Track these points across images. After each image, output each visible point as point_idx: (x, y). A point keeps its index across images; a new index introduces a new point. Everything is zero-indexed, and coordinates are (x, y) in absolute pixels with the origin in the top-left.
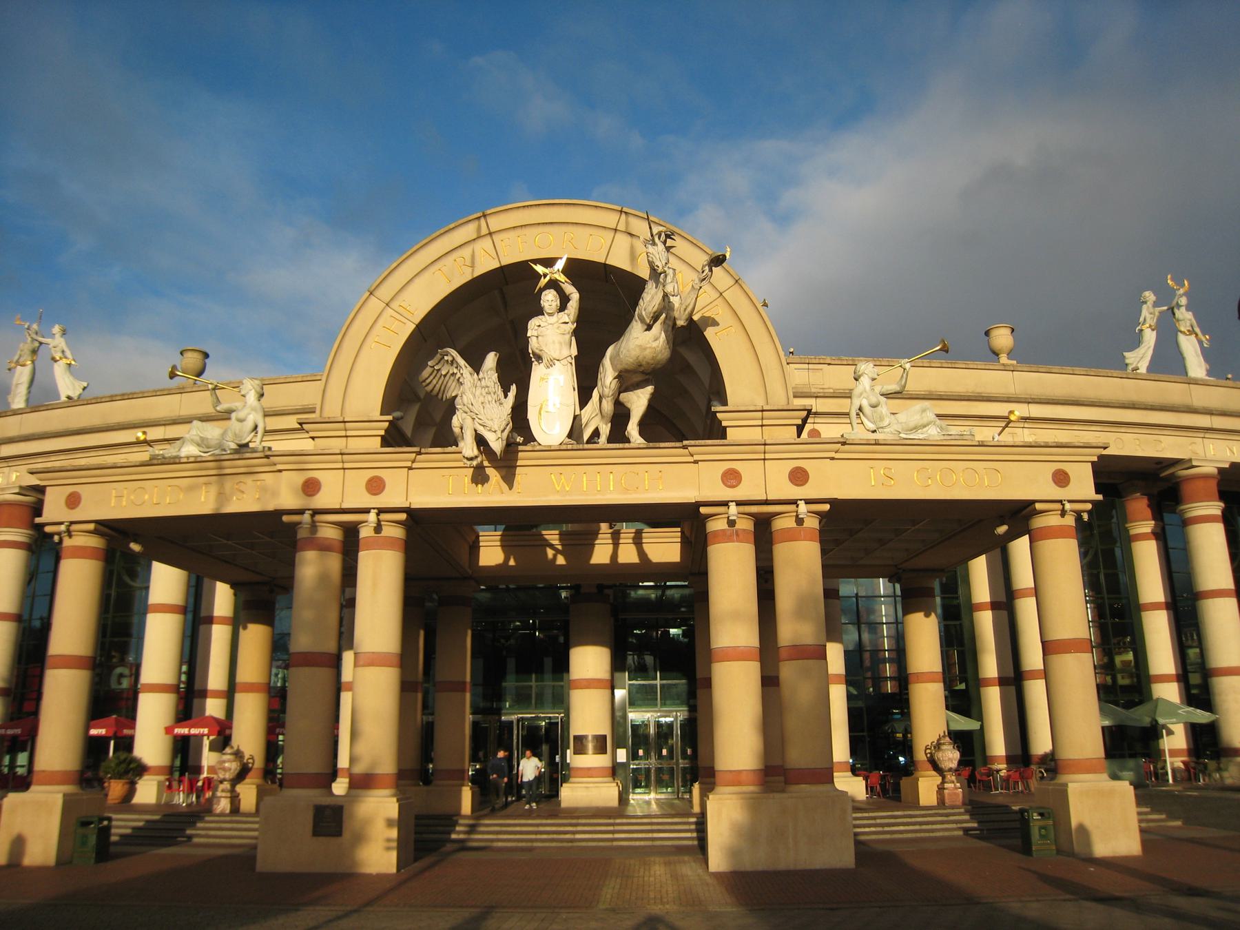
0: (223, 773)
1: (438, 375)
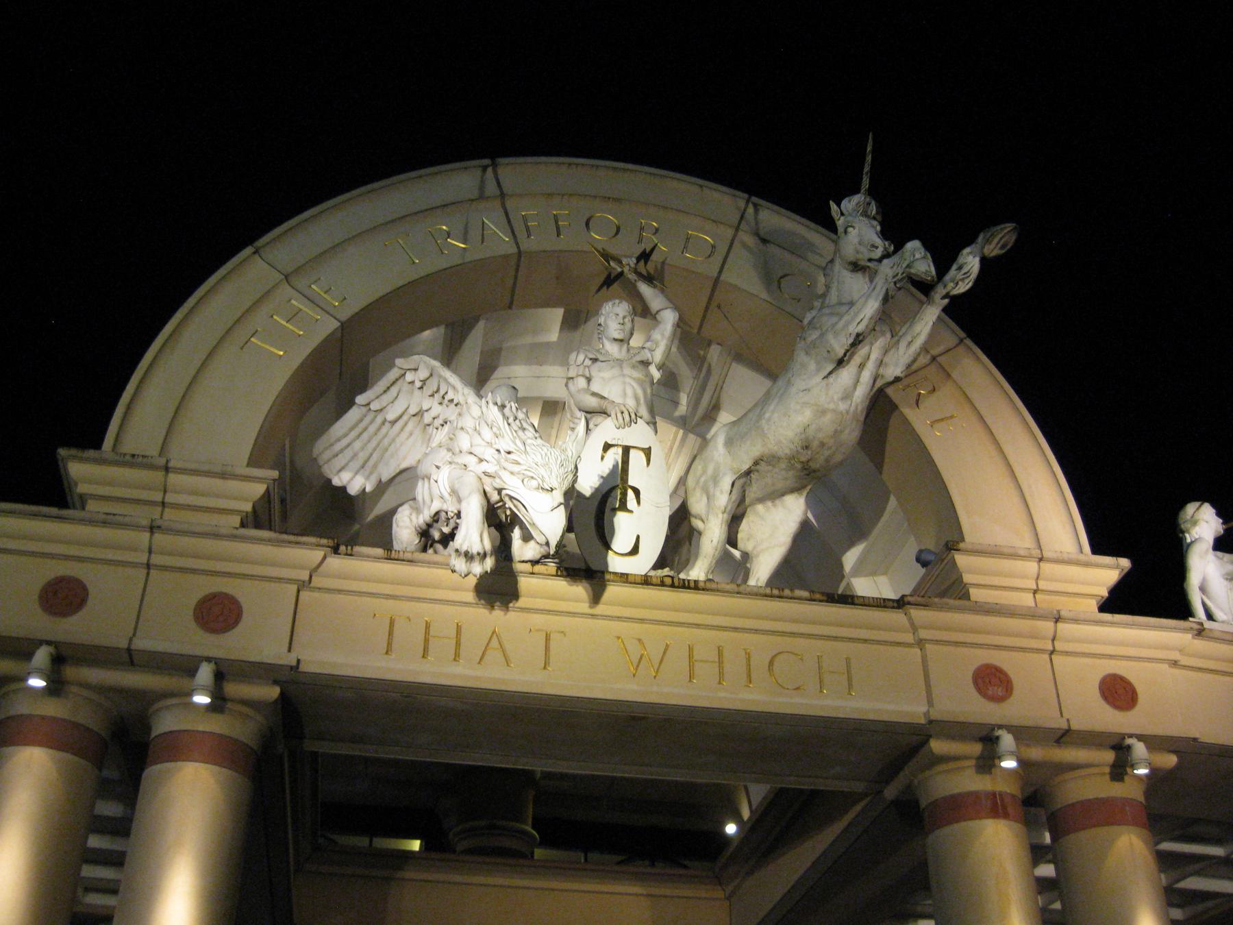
1: (379, 419)
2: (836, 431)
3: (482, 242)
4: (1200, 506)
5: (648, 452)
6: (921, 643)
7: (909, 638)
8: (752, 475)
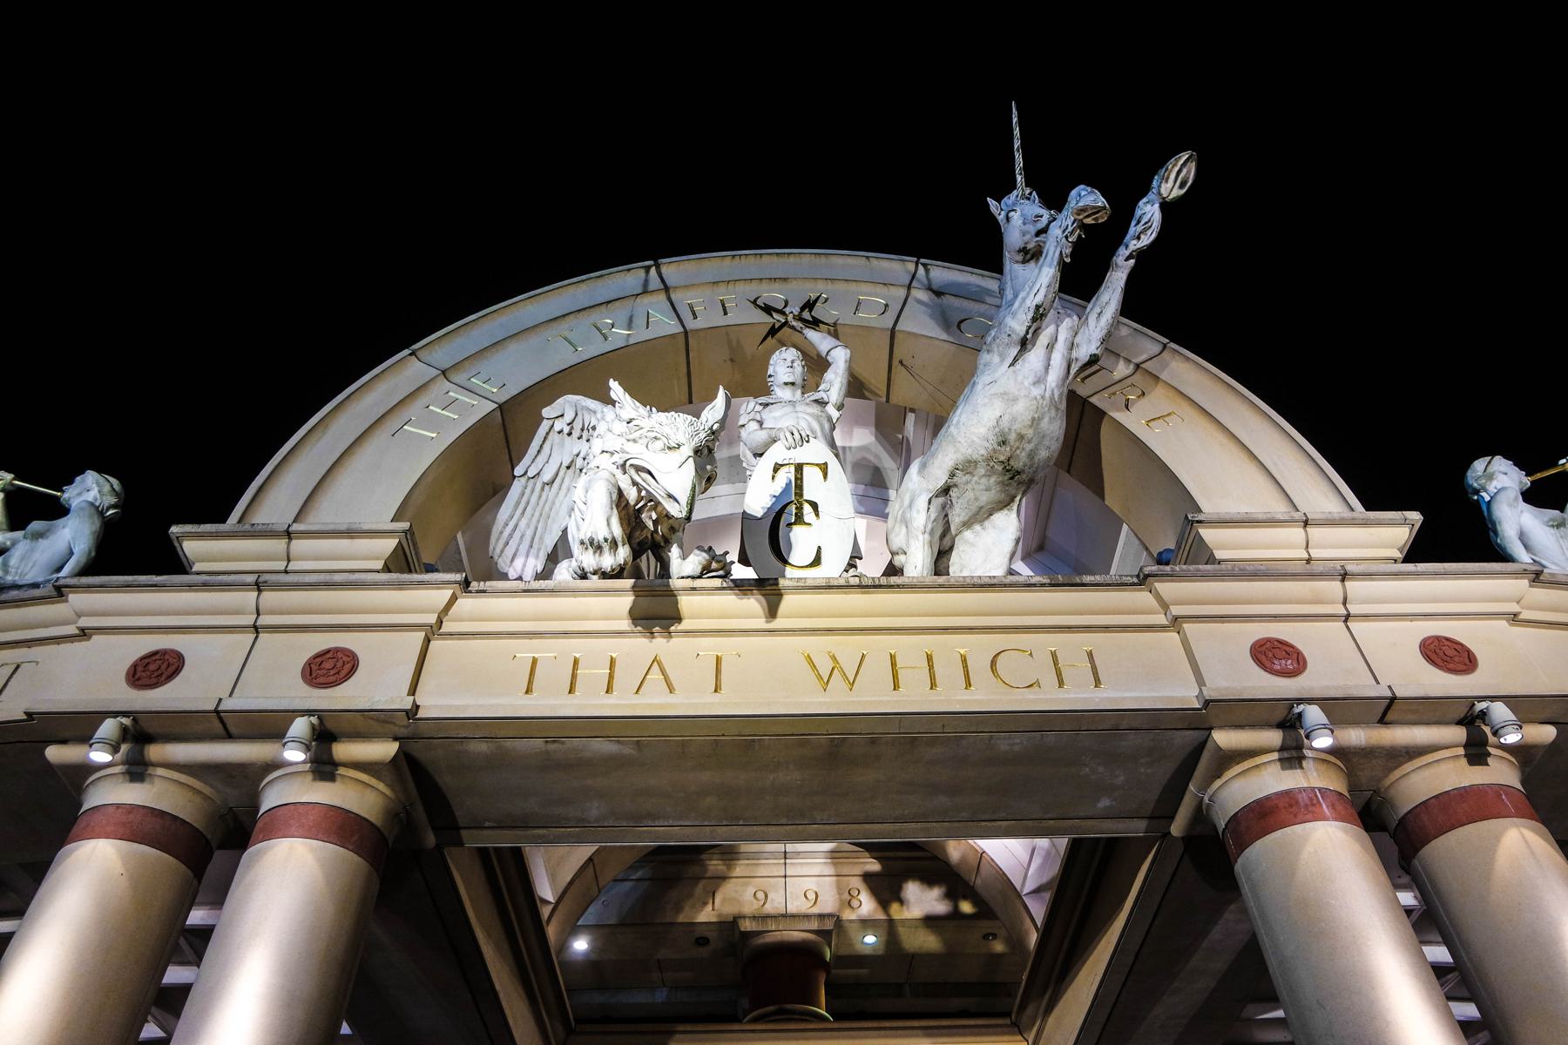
2: (1033, 419)
3: (647, 328)
4: (1492, 459)
5: (824, 468)
6: (1176, 622)
7: (1161, 619)
8: (951, 493)
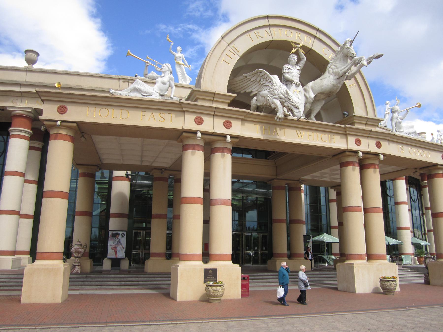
0: (77, 254)
